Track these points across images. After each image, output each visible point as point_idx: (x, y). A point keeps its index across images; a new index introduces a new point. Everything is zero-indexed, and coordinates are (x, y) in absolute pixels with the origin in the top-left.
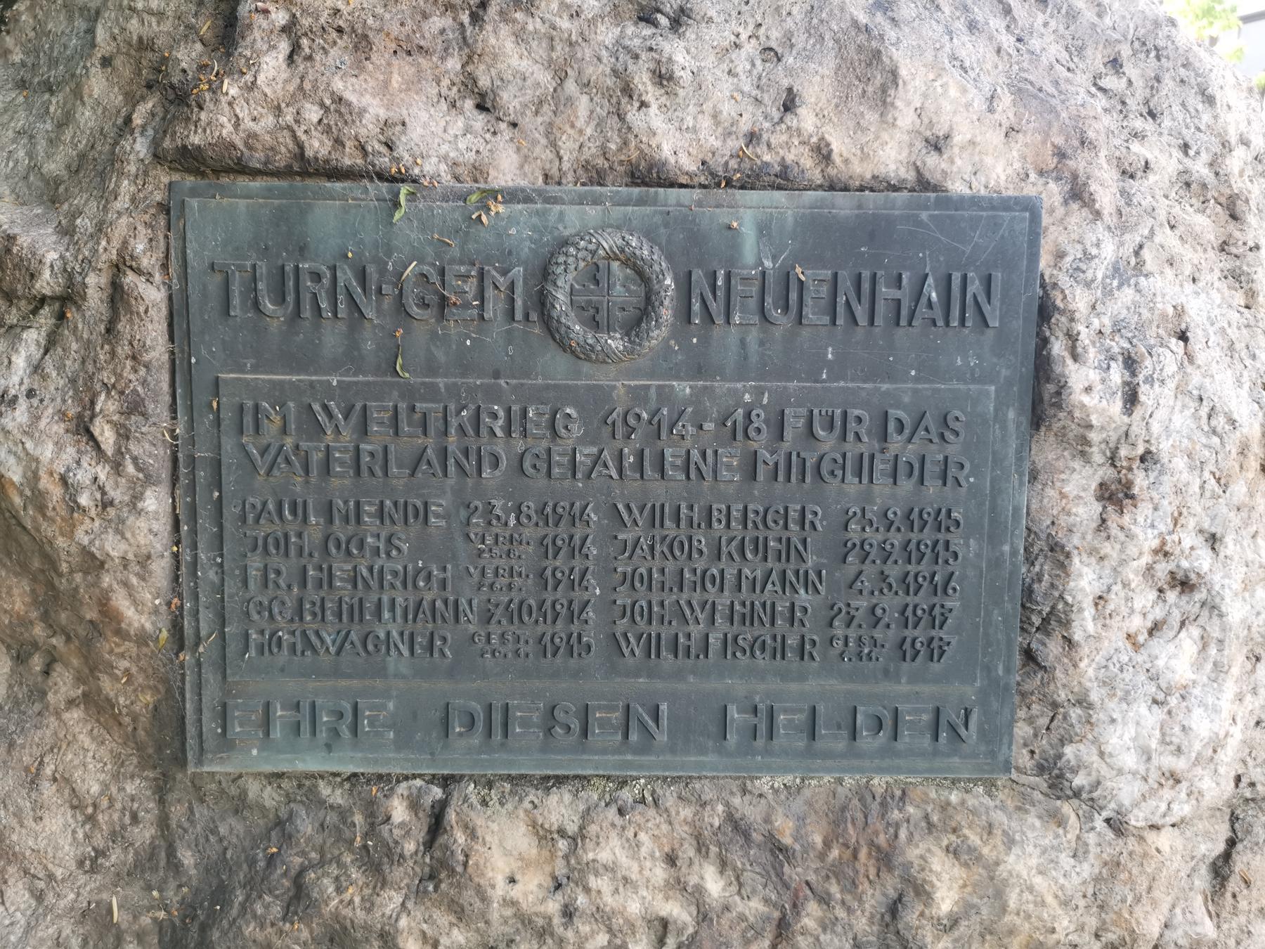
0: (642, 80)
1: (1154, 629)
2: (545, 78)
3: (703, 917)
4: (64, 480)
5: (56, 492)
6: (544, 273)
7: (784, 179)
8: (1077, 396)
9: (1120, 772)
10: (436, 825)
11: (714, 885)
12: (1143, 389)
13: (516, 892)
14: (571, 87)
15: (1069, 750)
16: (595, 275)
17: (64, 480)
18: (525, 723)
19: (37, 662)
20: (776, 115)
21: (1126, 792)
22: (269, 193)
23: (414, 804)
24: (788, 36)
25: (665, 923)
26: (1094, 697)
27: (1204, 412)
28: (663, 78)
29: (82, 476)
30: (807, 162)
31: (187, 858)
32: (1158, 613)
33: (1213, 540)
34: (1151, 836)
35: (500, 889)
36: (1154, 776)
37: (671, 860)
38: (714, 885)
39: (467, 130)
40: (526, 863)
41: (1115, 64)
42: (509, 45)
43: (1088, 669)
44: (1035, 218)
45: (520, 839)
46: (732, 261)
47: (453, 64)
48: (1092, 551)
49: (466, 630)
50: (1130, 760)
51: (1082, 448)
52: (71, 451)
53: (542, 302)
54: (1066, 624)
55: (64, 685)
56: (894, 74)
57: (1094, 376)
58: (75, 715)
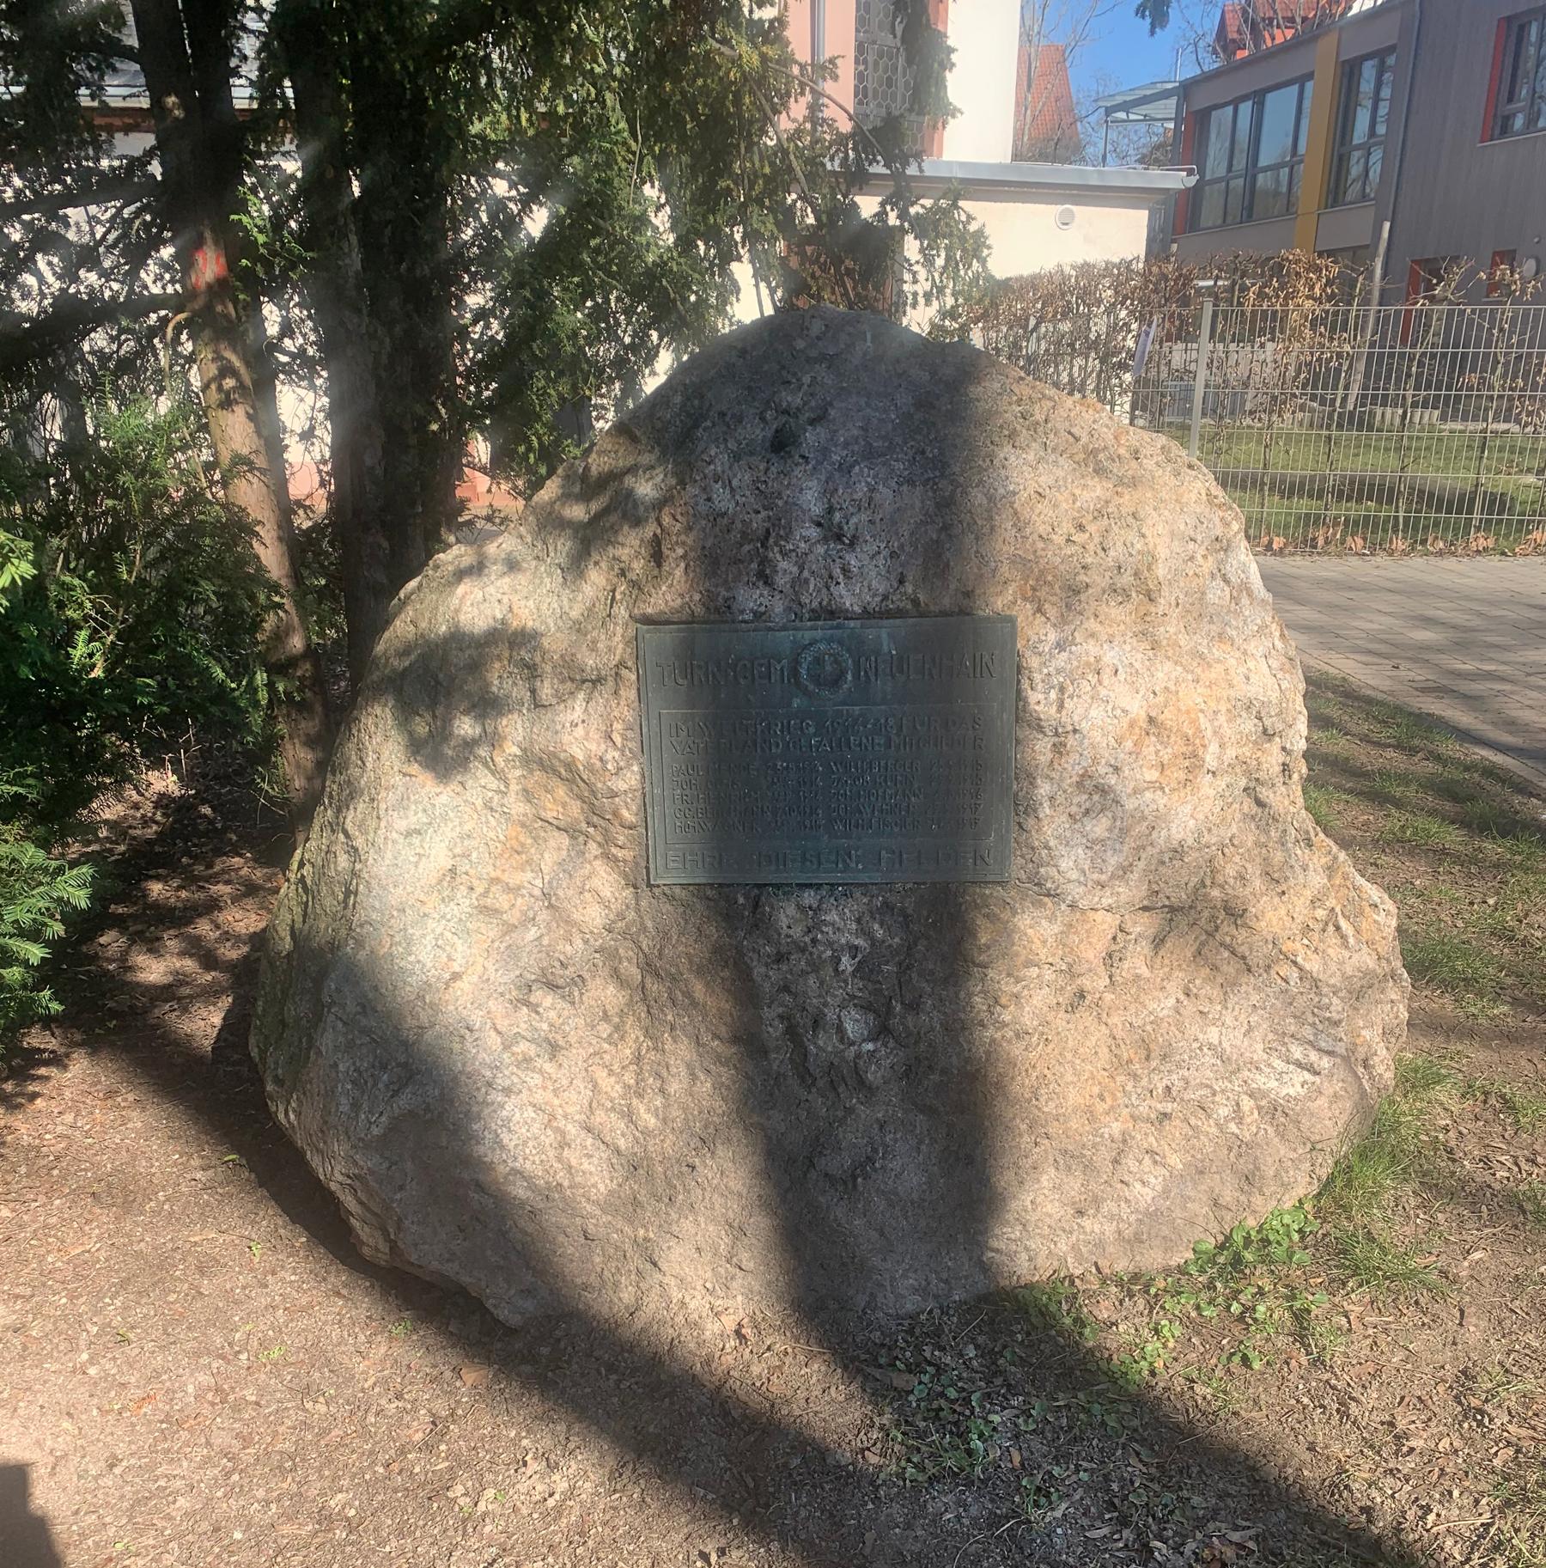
0: (837, 572)
1: (1087, 812)
2: (795, 570)
3: (873, 945)
4: (601, 759)
5: (598, 764)
6: (796, 663)
7: (900, 613)
8: (1033, 706)
9: (1069, 881)
10: (756, 905)
11: (879, 933)
12: (1067, 701)
13: (791, 932)
14: (806, 574)
15: (1042, 870)
16: (818, 661)
17: (601, 759)
18: (793, 861)
19: (581, 839)
20: (895, 585)
21: (1076, 891)
22: (679, 631)
23: (746, 897)
24: (902, 547)
25: (856, 948)
26: (1052, 843)
27: (1109, 708)
28: (845, 571)
29: (609, 757)
30: (909, 606)
31: (649, 924)
32: (1088, 805)
33: (1117, 769)
34: (1091, 914)
35: (785, 930)
36: (1090, 884)
37: (858, 921)
38: (879, 933)
39: (761, 595)
40: (796, 921)
41: (1081, 528)
42: (779, 557)
43: (1048, 830)
44: (1014, 626)
45: (791, 910)
46: (877, 653)
47: (754, 566)
48: (1048, 777)
49: (467, 225)
50: (1074, 875)
51: (1040, 729)
52: (603, 747)
53: (795, 673)
54: (1035, 811)
55: (594, 850)
56: (947, 565)
57: (1041, 697)
58: (597, 863)
